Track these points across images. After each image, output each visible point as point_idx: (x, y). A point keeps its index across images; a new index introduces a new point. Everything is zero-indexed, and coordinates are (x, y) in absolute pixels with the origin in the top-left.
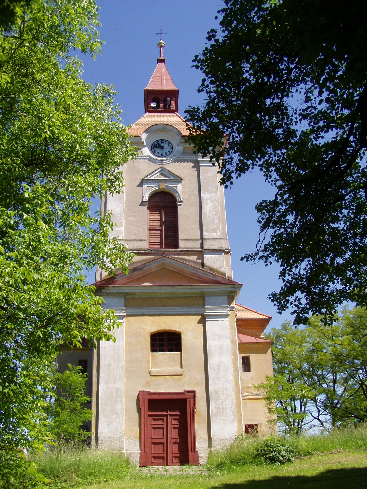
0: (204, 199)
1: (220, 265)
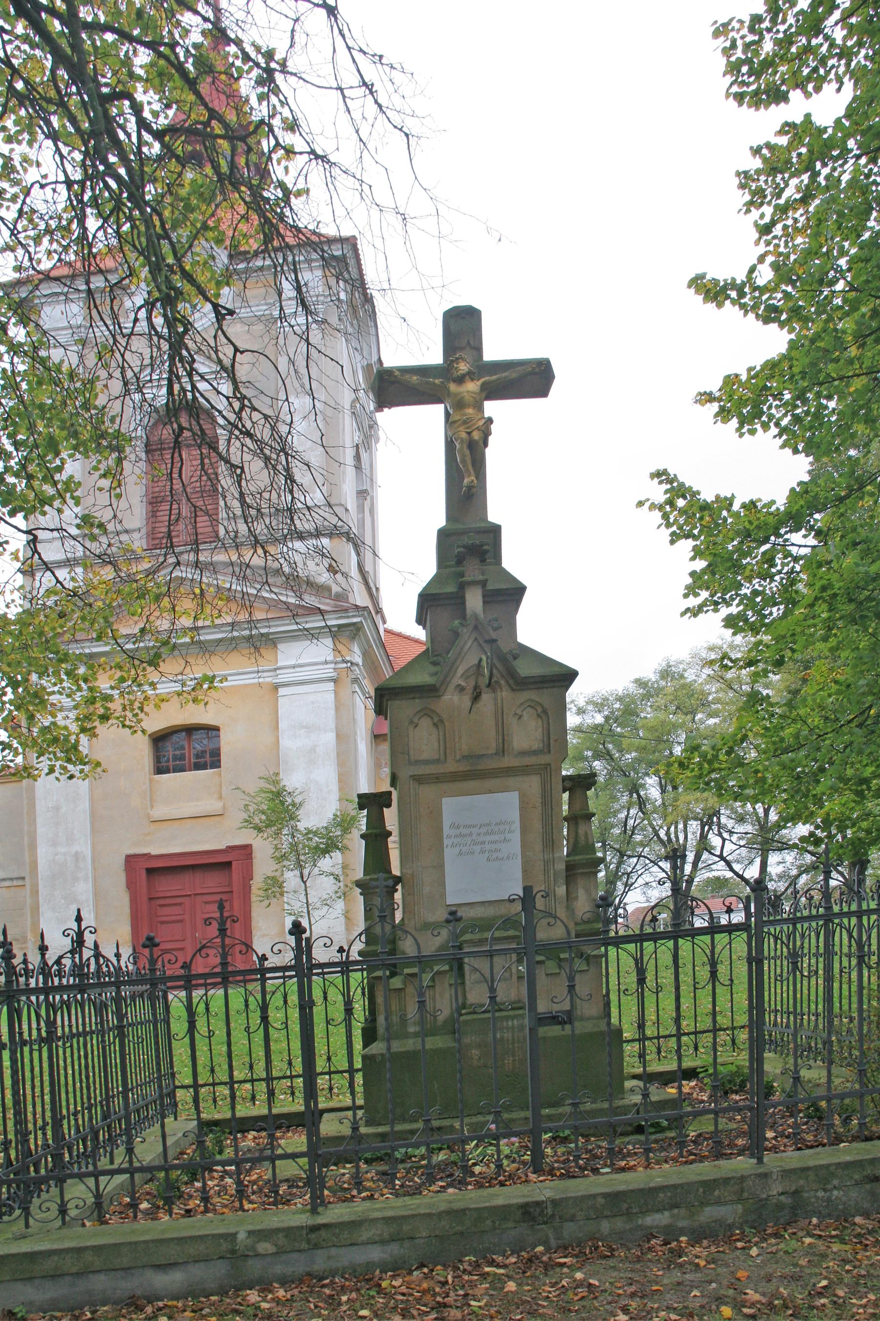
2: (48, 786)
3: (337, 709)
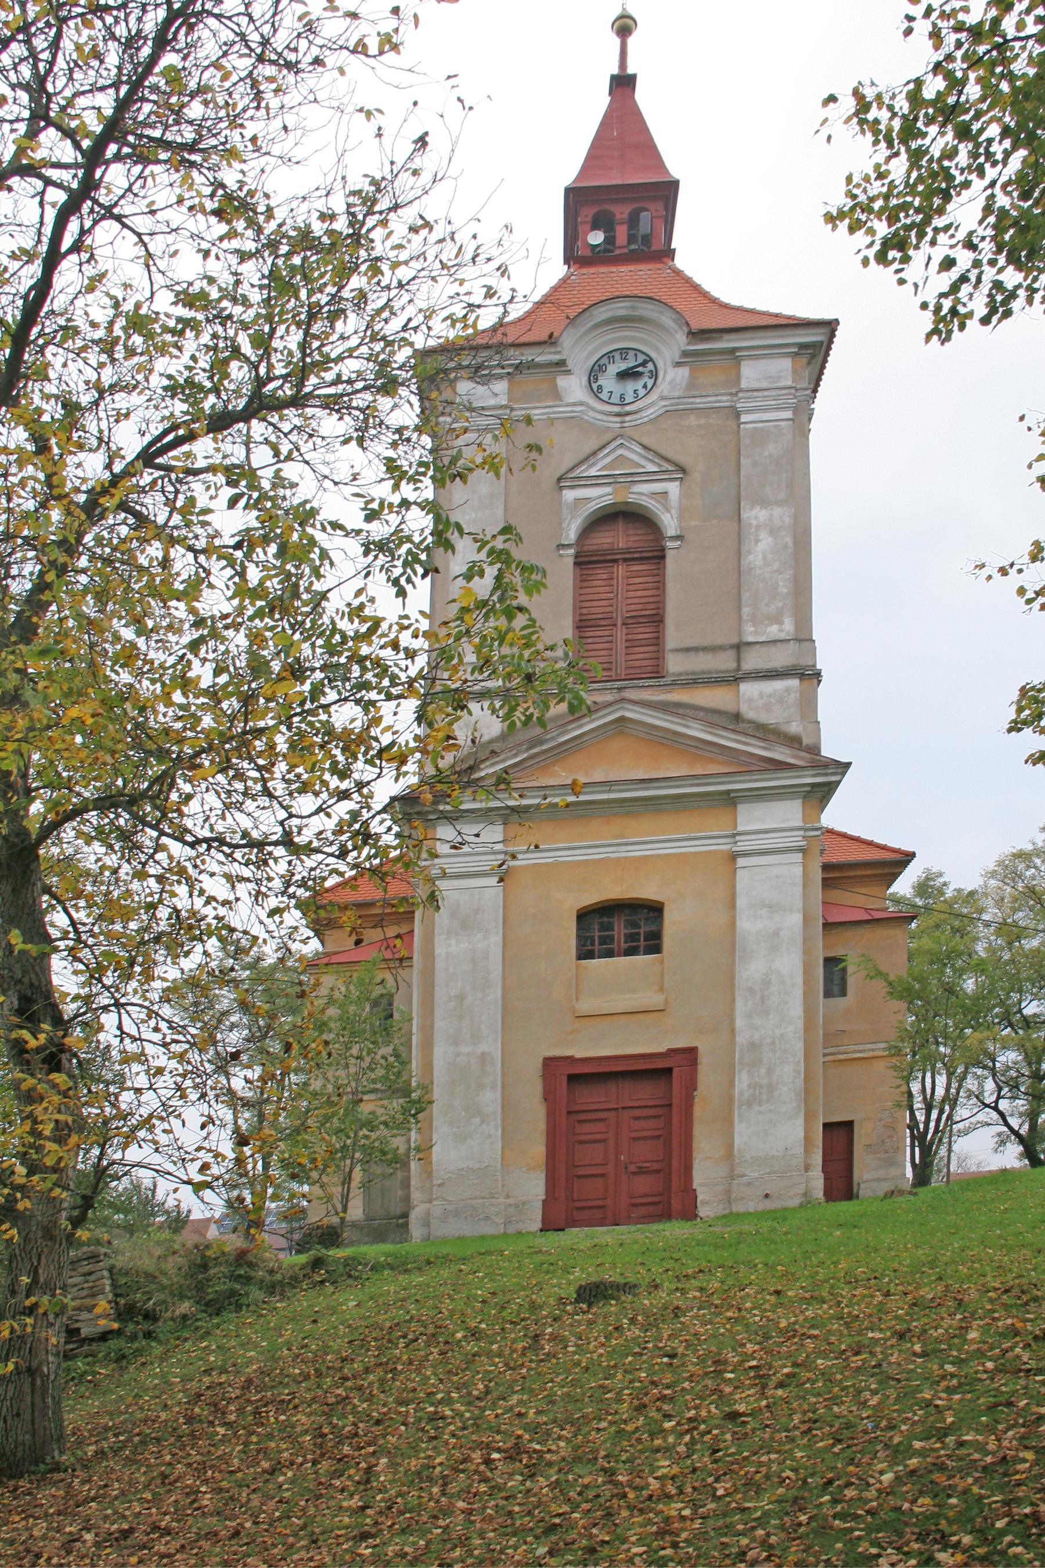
0: (750, 525)
2: (451, 970)
3: (805, 886)
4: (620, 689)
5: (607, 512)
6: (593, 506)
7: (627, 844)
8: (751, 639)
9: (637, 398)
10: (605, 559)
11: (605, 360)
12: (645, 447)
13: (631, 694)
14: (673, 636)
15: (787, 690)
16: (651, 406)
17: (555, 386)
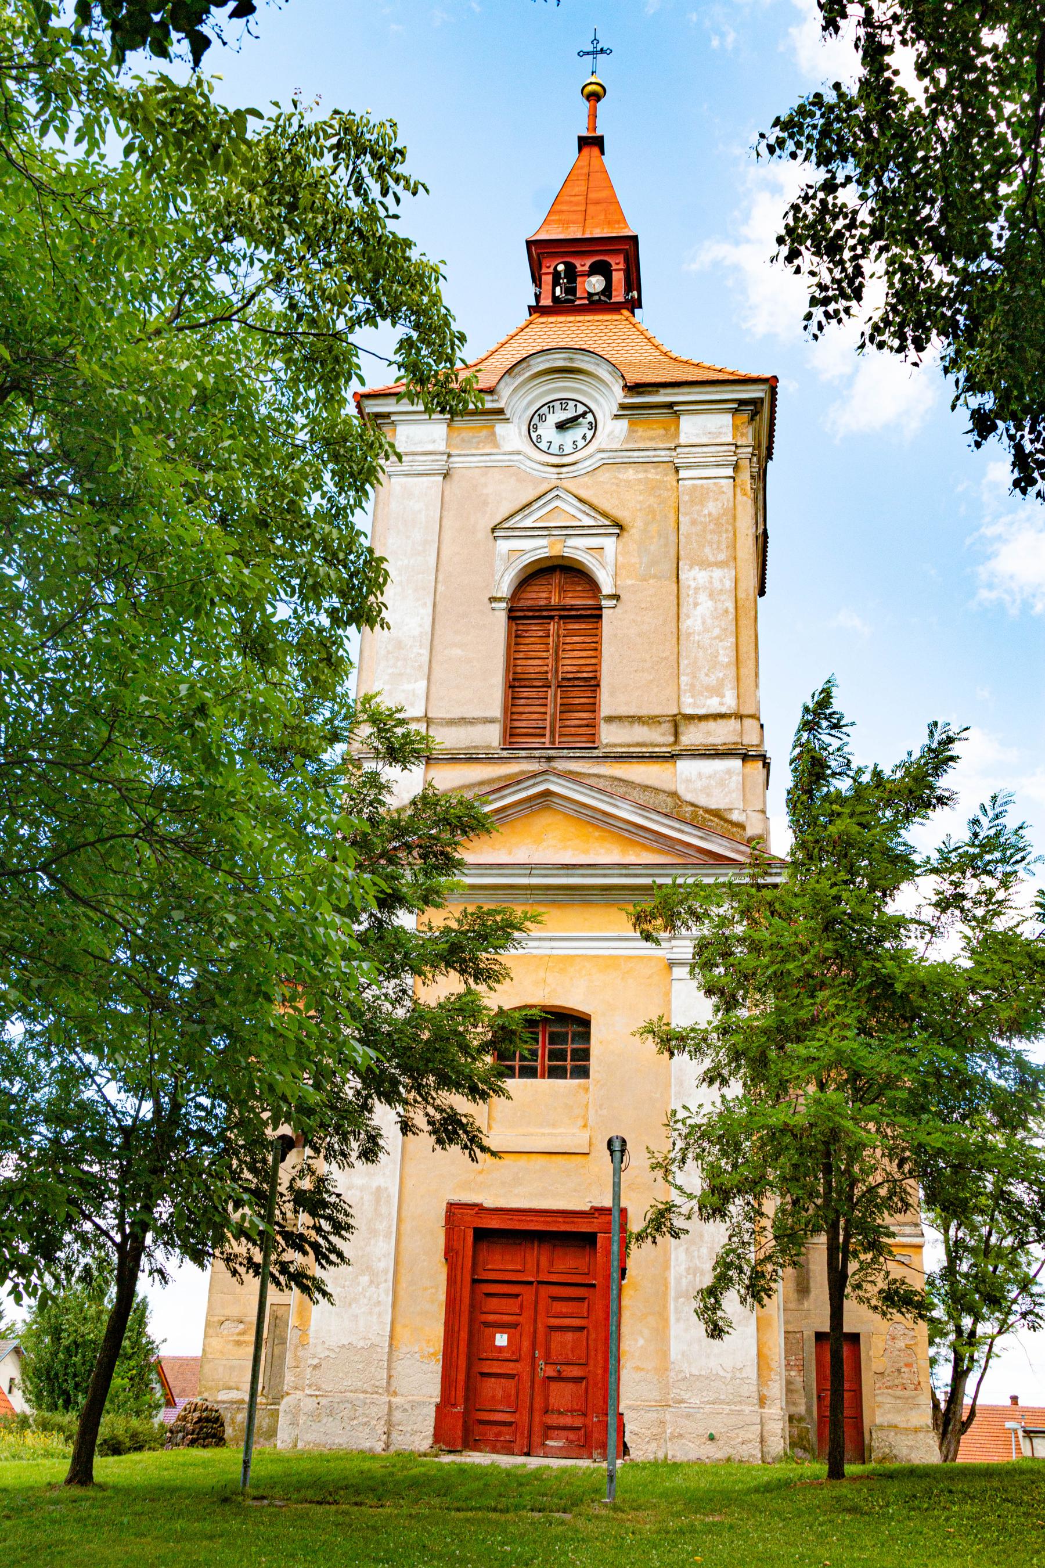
0: (689, 587)
1: (727, 800)
4: (549, 759)
5: (544, 565)
6: (527, 559)
7: (551, 939)
8: (689, 711)
9: (576, 449)
10: (542, 615)
11: (545, 409)
12: (581, 500)
13: (560, 765)
14: (607, 705)
15: (729, 772)
16: (588, 458)
17: (494, 434)
